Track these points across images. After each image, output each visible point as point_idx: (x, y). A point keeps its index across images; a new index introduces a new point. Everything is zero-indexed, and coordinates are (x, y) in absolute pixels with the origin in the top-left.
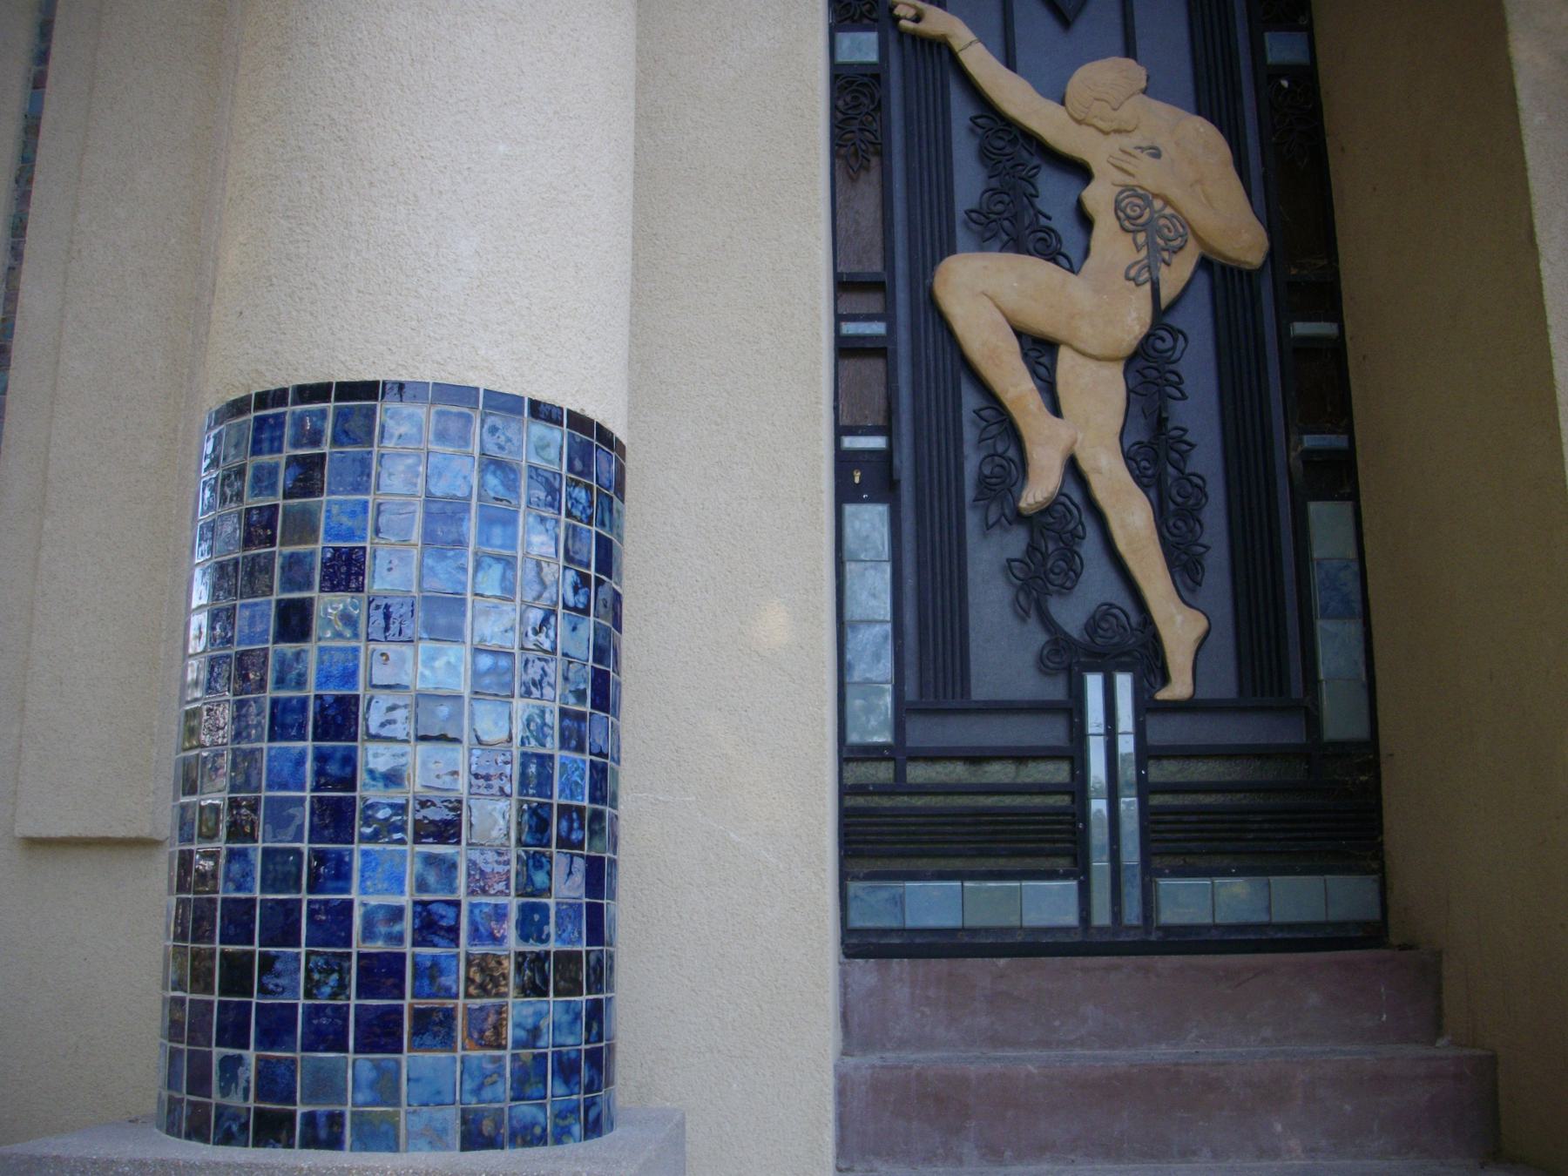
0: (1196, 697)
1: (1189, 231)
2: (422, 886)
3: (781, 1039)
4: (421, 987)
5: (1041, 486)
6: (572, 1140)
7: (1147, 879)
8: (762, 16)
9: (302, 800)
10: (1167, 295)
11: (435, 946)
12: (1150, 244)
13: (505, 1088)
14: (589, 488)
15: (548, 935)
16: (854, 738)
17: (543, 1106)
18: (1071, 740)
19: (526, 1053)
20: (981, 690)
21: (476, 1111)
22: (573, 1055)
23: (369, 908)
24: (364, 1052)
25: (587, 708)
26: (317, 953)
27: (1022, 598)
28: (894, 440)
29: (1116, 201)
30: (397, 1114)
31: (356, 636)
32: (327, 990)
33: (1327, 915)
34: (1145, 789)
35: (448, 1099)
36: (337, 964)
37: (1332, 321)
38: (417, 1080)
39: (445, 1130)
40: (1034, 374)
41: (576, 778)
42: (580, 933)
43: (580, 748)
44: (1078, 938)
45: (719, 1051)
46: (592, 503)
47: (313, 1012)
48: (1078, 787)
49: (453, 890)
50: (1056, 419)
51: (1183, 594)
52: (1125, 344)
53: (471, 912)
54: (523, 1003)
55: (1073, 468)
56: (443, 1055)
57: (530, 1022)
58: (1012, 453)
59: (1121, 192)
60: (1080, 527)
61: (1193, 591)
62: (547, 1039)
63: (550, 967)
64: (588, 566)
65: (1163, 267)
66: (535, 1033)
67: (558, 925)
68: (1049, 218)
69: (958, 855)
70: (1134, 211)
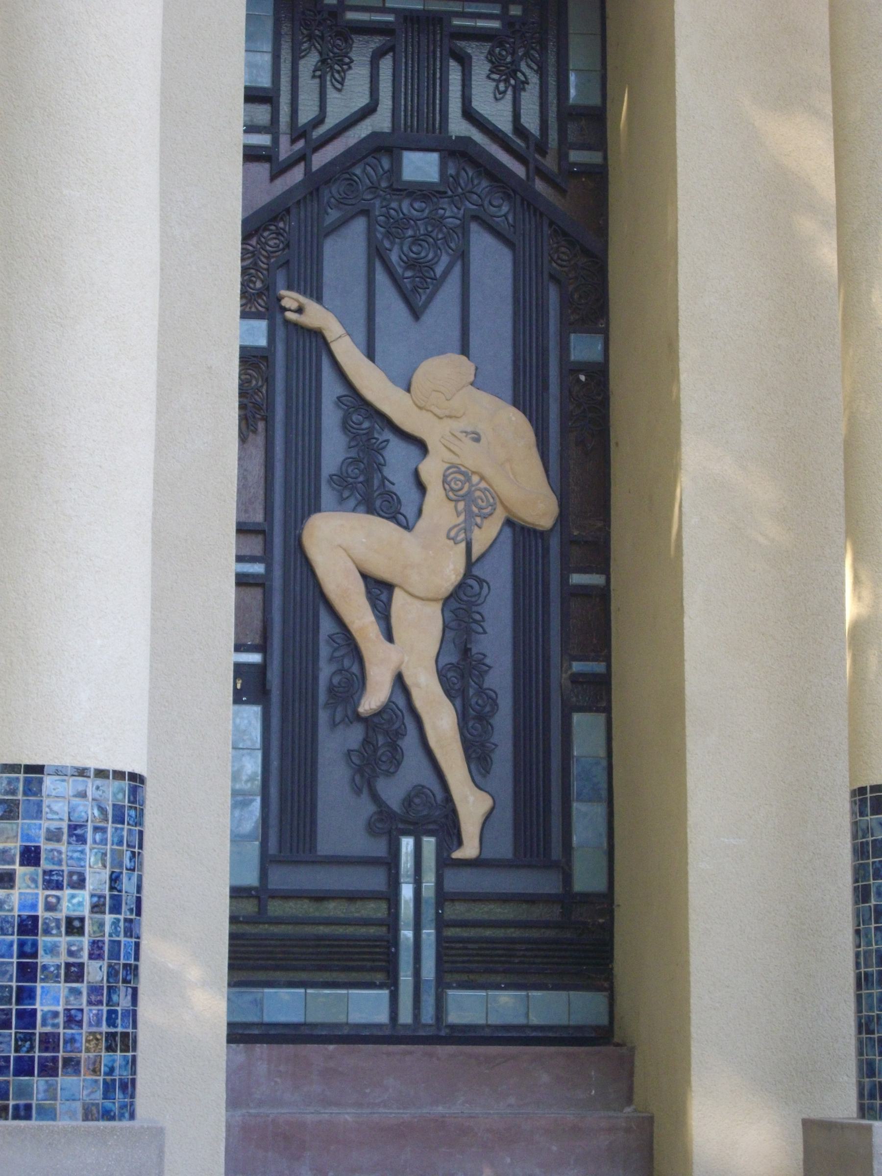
1: (497, 500)
7: (440, 990)
8: (199, 426)
9: (12, 963)
10: (476, 551)
11: (72, 1029)
12: (469, 515)
17: (114, 1103)
18: (389, 885)
19: (108, 1078)
20: (324, 847)
21: (88, 1104)
26: (20, 1033)
27: (357, 778)
28: (268, 657)
29: (444, 476)
31: (37, 887)
32: (25, 1049)
34: (441, 924)
36: (30, 1037)
37: (602, 573)
40: (374, 606)
41: (129, 951)
43: (131, 936)
44: (388, 1032)
45: (159, 1096)
47: (18, 1060)
48: (392, 923)
51: (475, 778)
52: (443, 590)
55: (399, 680)
57: (110, 1065)
58: (355, 669)
59: (448, 469)
60: (403, 727)
61: (484, 776)
62: (117, 1072)
63: (118, 1039)
64: (135, 847)
65: (476, 530)
67: (122, 1019)
68: (393, 484)
69: (304, 969)
70: (457, 485)
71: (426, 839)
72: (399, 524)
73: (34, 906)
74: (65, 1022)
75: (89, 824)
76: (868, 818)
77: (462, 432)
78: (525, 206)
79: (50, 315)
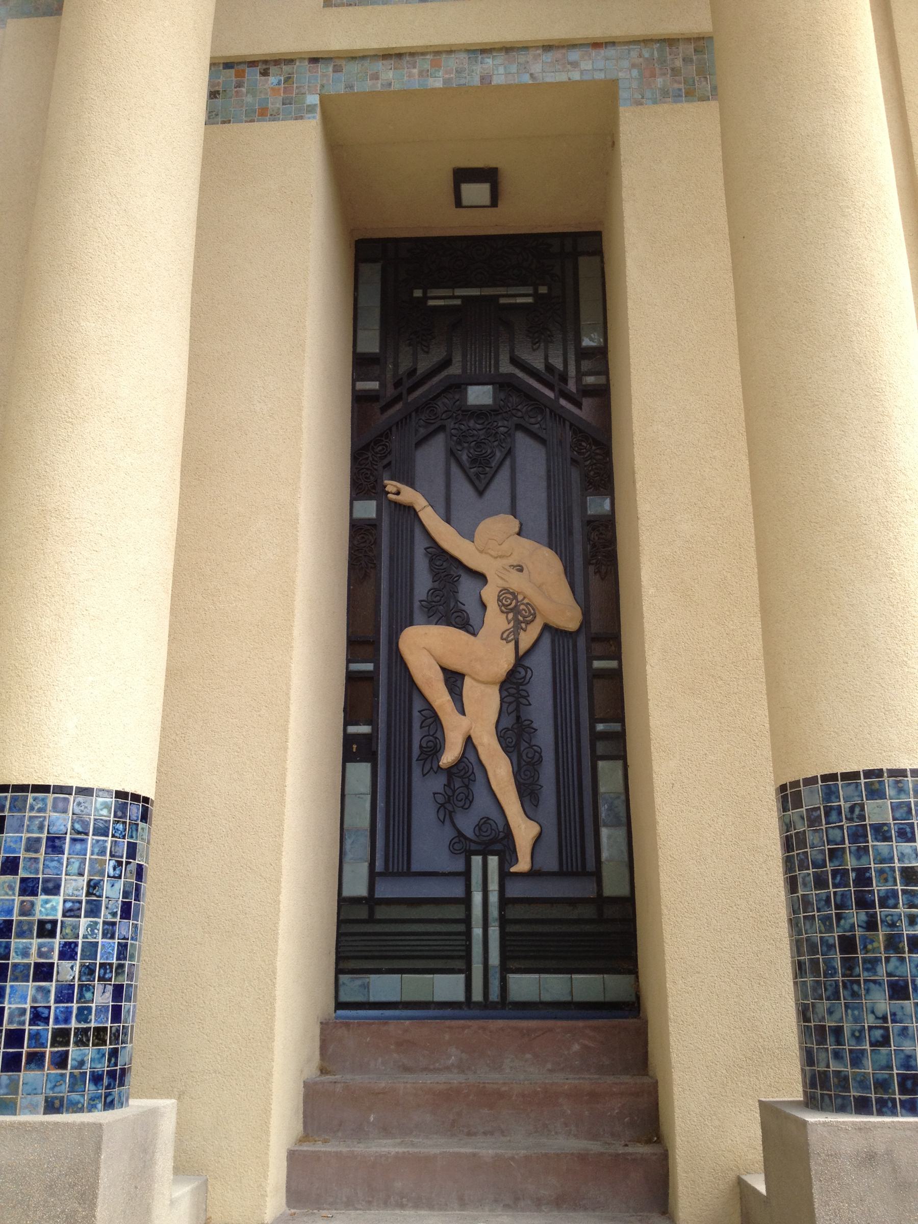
0: (534, 869)
2: (34, 1000)
3: (250, 1066)
4: (32, 1043)
5: (449, 757)
6: (97, 1110)
11: (39, 1026)
12: (516, 619)
13: (65, 1087)
14: (124, 823)
15: (91, 1020)
16: (346, 893)
21: (52, 1097)
22: (100, 1073)
23: (11, 1009)
24: (5, 1072)
25: (118, 919)
30: (17, 1098)
33: (605, 997)
34: (503, 921)
35: (40, 1092)
38: (26, 1084)
39: (37, 1106)
41: (110, 950)
42: (107, 1019)
46: (125, 829)
48: (467, 921)
49: (49, 1002)
50: (462, 717)
53: (55, 1011)
54: (76, 1050)
55: (469, 741)
56: (39, 1073)
57: (79, 1059)
64: (122, 857)
66: (82, 1063)
68: (464, 605)
71: (490, 858)
72: (468, 631)
73: (10, 912)
74: (30, 1020)
75: (68, 836)
76: (790, 813)
77: (510, 566)
78: (558, 419)
79: (63, 416)
